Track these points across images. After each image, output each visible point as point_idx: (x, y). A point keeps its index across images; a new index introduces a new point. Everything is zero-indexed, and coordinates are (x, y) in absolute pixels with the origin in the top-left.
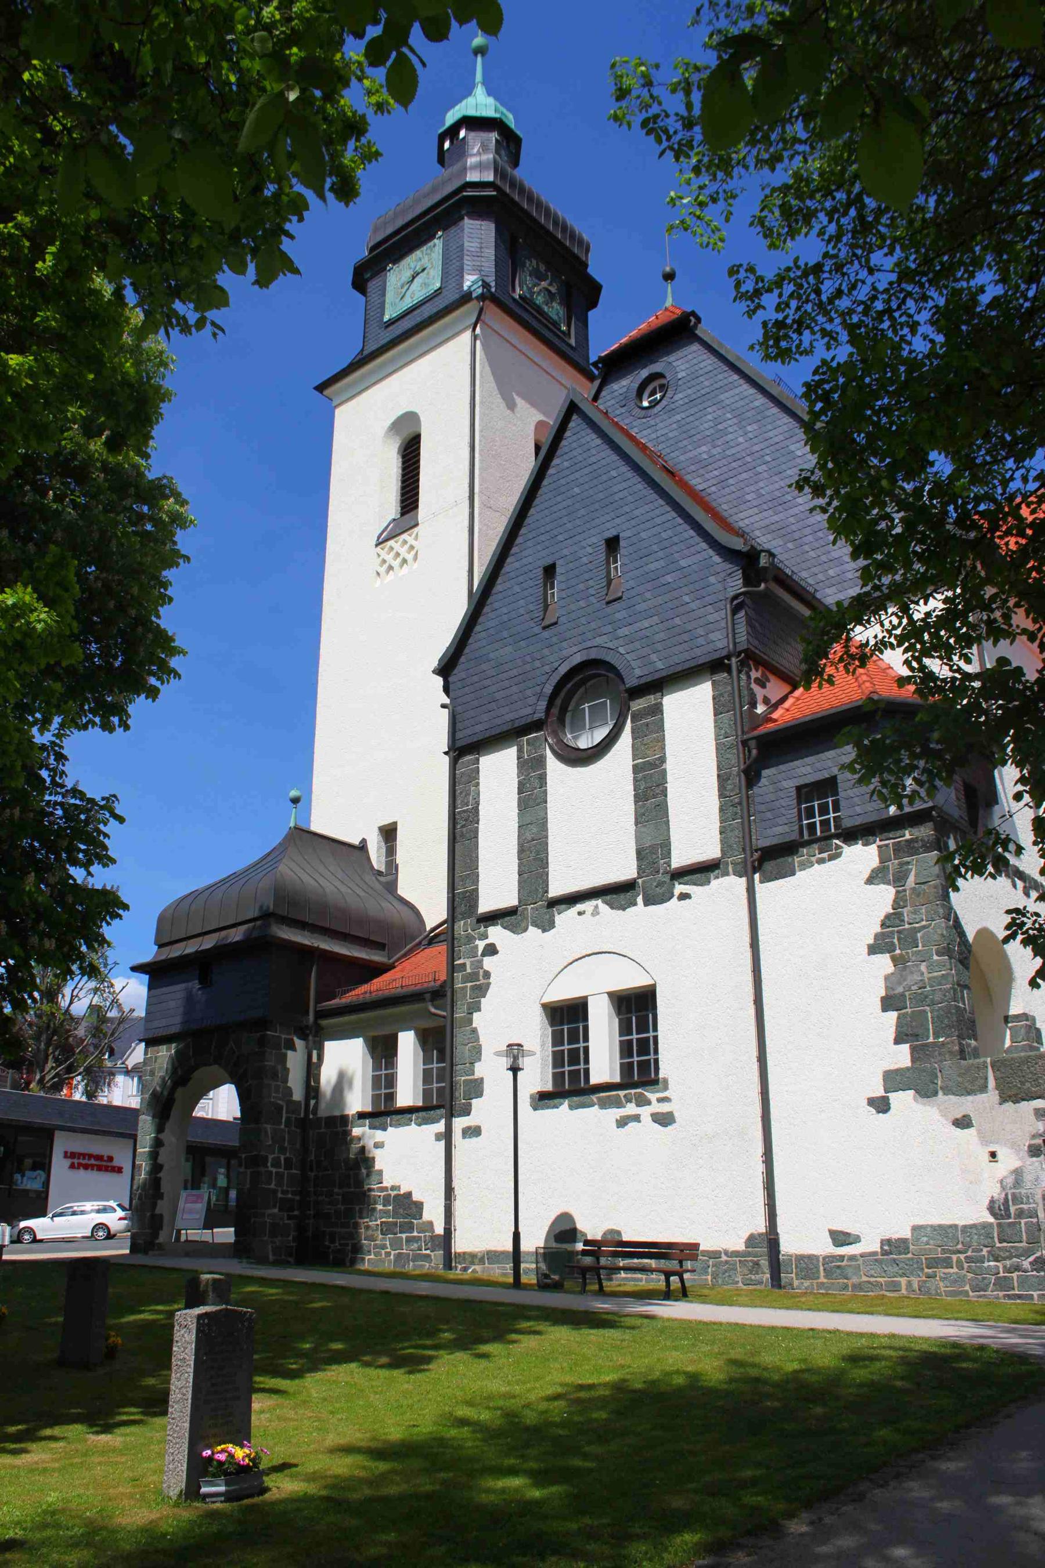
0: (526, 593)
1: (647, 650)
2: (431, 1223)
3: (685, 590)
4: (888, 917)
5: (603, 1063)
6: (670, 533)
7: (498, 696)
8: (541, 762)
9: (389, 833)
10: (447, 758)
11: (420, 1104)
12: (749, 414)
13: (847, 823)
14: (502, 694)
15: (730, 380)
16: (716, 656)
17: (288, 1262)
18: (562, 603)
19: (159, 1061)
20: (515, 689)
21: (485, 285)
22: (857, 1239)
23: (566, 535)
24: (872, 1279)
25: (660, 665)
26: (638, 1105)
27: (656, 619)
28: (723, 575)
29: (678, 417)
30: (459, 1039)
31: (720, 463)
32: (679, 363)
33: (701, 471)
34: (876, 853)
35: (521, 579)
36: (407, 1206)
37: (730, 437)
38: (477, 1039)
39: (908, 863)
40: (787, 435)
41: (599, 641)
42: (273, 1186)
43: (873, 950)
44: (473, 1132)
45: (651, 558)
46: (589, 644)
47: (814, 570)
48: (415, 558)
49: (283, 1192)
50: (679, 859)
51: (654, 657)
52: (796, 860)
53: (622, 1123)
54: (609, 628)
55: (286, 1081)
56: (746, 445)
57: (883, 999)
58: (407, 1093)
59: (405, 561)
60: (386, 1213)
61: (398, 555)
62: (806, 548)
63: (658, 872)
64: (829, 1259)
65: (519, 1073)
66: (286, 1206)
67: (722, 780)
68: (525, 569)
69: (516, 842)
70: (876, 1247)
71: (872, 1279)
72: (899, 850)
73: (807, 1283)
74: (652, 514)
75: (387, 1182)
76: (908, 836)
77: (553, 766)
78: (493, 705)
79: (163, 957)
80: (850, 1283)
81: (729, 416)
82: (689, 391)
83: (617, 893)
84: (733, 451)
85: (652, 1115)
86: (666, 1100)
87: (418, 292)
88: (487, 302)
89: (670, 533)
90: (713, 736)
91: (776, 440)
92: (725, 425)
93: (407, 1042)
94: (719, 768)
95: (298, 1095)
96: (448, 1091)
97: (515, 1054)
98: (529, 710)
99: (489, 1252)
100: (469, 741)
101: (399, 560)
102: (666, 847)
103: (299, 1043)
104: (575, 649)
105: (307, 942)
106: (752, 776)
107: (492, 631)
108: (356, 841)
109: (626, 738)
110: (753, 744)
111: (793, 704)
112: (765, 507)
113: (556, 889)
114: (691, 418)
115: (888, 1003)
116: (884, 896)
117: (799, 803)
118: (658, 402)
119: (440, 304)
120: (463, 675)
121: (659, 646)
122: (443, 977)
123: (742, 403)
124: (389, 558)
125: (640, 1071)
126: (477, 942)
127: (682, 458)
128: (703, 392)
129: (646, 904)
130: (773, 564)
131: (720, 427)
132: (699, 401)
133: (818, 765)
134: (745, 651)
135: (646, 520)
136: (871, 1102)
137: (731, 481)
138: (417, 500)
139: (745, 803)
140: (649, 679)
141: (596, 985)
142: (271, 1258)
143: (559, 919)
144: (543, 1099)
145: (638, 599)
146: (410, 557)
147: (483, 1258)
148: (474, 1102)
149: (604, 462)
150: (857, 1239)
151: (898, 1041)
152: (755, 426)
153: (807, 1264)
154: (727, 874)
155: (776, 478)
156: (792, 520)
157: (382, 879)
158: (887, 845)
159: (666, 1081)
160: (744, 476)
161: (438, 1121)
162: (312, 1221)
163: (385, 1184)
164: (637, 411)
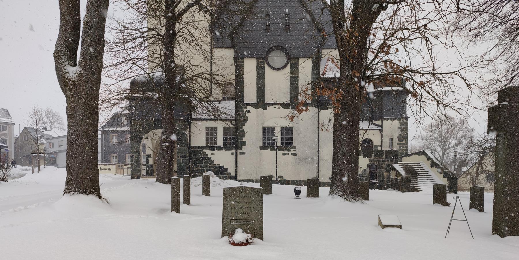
8: (263, 68)
44: (297, 193)
53: (284, 154)
75: (215, 163)
86: (295, 151)
109: (289, 67)
143: (268, 107)
148: (243, 147)
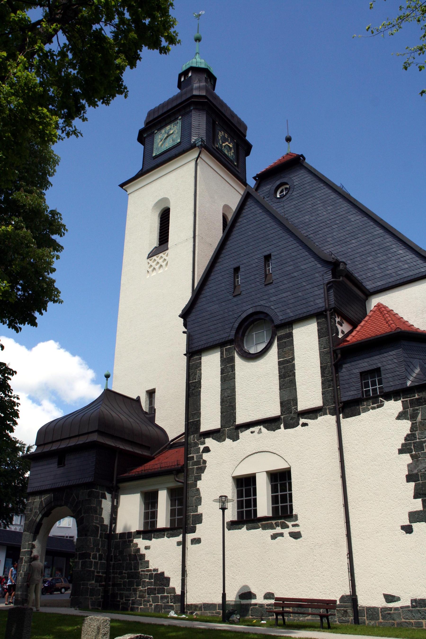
0: (225, 280)
1: (285, 307)
2: (174, 589)
3: (304, 279)
4: (408, 435)
5: (264, 507)
6: (295, 253)
7: (211, 328)
8: (232, 360)
9: (151, 393)
10: (185, 357)
11: (169, 527)
12: (328, 202)
13: (386, 390)
14: (213, 327)
15: (319, 186)
16: (319, 310)
17: (98, 609)
18: (243, 285)
19: (35, 504)
20: (220, 325)
21: (202, 141)
22: (398, 599)
23: (244, 254)
24: (407, 621)
25: (291, 314)
26: (282, 528)
27: (289, 293)
28: (322, 273)
29: (294, 203)
30: (190, 493)
31: (314, 224)
32: (295, 178)
33: (306, 227)
34: (401, 404)
35: (223, 273)
36: (162, 580)
37: (320, 212)
38: (199, 494)
39: (417, 410)
40: (346, 211)
41: (262, 303)
42: (92, 569)
43: (401, 451)
44: (196, 541)
45: (287, 265)
46: (256, 304)
47: (361, 273)
48: (167, 264)
49: (98, 572)
50: (302, 406)
51: (288, 311)
52: (361, 407)
53: (274, 537)
54: (266, 297)
55: (101, 514)
56: (327, 216)
57: (407, 476)
58: (162, 520)
59: (161, 266)
60: (150, 583)
61: (158, 263)
62: (357, 263)
63: (291, 413)
64: (384, 609)
65: (226, 511)
66: (98, 579)
67: (323, 369)
68: (225, 269)
69: (219, 397)
70: (409, 604)
71: (407, 621)
72: (412, 403)
73: (373, 622)
74: (287, 245)
75: (152, 567)
76: (417, 397)
77: (239, 362)
78: (208, 333)
79: (40, 451)
80: (395, 622)
81: (319, 202)
82: (300, 191)
83: (271, 423)
84: (321, 218)
85: (289, 533)
87: (169, 144)
88: (203, 149)
89: (295, 253)
90: (318, 348)
91: (342, 213)
92: (317, 206)
93: (163, 497)
94: (321, 363)
95: (107, 522)
96: (184, 520)
97: (223, 501)
98: (226, 335)
99: (204, 604)
100: (197, 349)
101: (159, 265)
102: (295, 401)
103: (108, 496)
104: (249, 307)
105: (113, 445)
106: (338, 367)
107: (208, 298)
108: (135, 398)
109: (274, 349)
110: (339, 352)
111: (356, 334)
112: (336, 244)
113: (240, 420)
114: (301, 203)
115: (409, 478)
116: (405, 426)
117: (361, 381)
118: (284, 196)
119: (180, 149)
120: (194, 318)
121: (291, 306)
122: (182, 463)
123: (325, 197)
124: (154, 264)
125: (283, 510)
126: (200, 446)
127: (296, 221)
128: (306, 191)
129: (286, 428)
130: (346, 268)
131: (315, 207)
132: (304, 195)
133: (371, 362)
134: (334, 308)
135: (284, 249)
136: (403, 528)
137: (320, 232)
138: (168, 238)
139: (335, 381)
140: (287, 321)
141: (260, 468)
142: (90, 607)
143: (241, 435)
144: (233, 525)
145: (281, 284)
146: (164, 264)
147: (201, 607)
148: (198, 526)
149: (263, 220)
150: (398, 599)
151: (415, 497)
152: (331, 207)
153: (372, 612)
154: (326, 414)
155: (341, 231)
156: (349, 250)
157: (147, 416)
158: (406, 401)
159: (296, 516)
160: (327, 230)
161: (178, 536)
162: (111, 587)
163: (150, 568)
164: (274, 199)
